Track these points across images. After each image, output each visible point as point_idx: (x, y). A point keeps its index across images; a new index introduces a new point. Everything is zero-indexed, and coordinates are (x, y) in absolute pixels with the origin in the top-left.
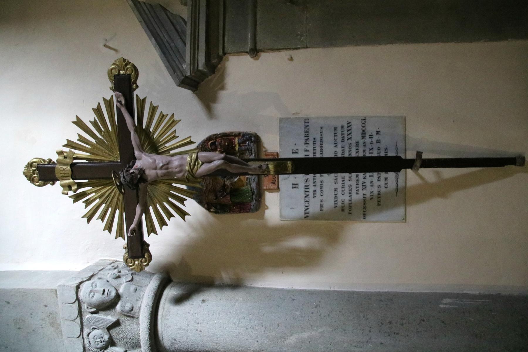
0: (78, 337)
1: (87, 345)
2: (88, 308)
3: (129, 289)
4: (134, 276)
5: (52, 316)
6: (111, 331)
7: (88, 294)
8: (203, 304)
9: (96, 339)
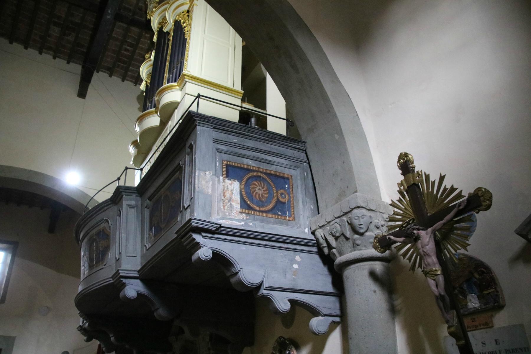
1: (331, 223)
3: (370, 239)
8: (372, 292)
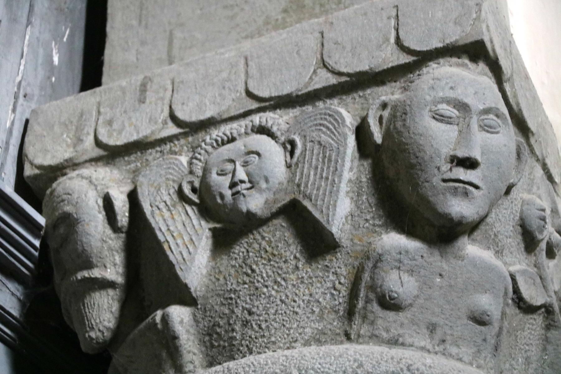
0: (250, 94)
1: (216, 133)
2: (384, 106)
4: (538, 320)
6: (280, 222)
9: (246, 164)
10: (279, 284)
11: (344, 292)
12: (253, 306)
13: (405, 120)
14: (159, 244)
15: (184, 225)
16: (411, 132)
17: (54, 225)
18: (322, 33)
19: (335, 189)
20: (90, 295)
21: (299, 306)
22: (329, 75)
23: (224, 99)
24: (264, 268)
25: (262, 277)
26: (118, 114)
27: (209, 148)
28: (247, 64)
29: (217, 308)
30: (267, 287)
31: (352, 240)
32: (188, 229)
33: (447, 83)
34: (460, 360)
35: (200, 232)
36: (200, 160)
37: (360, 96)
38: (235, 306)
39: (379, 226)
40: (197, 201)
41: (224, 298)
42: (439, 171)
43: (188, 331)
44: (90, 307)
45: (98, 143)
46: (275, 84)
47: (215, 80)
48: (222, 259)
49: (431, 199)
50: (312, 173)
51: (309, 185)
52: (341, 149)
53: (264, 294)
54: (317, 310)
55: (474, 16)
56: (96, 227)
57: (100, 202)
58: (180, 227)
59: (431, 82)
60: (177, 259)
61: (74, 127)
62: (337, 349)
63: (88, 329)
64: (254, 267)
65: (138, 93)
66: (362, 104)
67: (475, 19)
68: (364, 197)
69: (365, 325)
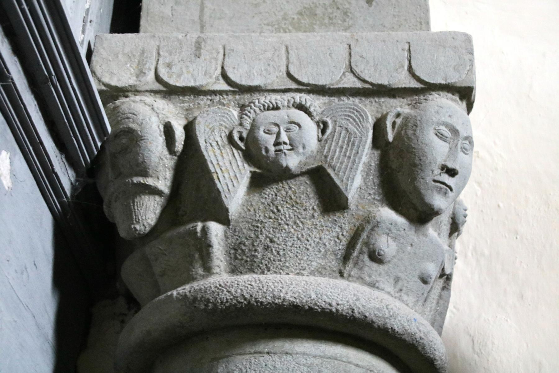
0: (290, 76)
2: (398, 115)
5: (338, 14)
6: (304, 179)
7: (449, 120)
9: (288, 130)
10: (298, 226)
11: (344, 242)
12: (275, 237)
13: (415, 131)
14: (209, 172)
15: (230, 163)
16: (419, 140)
17: (117, 135)
18: (350, 46)
19: (355, 167)
20: (141, 197)
21: (310, 245)
22: (355, 79)
23: (269, 74)
24: (287, 210)
25: (285, 217)
26: (176, 61)
27: (257, 110)
28: (288, 52)
29: (245, 231)
30: (288, 225)
31: (357, 206)
32: (234, 167)
33: (447, 112)
34: (407, 305)
35: (243, 172)
36: (249, 117)
37: (376, 102)
38: (259, 233)
39: (378, 200)
40: (244, 148)
41: (252, 225)
42: (432, 173)
43: (219, 243)
44: (139, 206)
45: (158, 78)
46: (312, 74)
47: (261, 57)
48: (255, 196)
49: (422, 191)
50: (338, 150)
51: (334, 159)
52: (364, 139)
53: (285, 230)
54: (323, 250)
55: (468, 68)
56: (157, 146)
57: (162, 128)
58: (228, 164)
59: (437, 108)
60: (223, 188)
61: (136, 60)
62: (333, 281)
63: (135, 222)
64: (280, 208)
65: (194, 49)
66: (377, 108)
67: (469, 71)
68: (371, 177)
69: (355, 269)
